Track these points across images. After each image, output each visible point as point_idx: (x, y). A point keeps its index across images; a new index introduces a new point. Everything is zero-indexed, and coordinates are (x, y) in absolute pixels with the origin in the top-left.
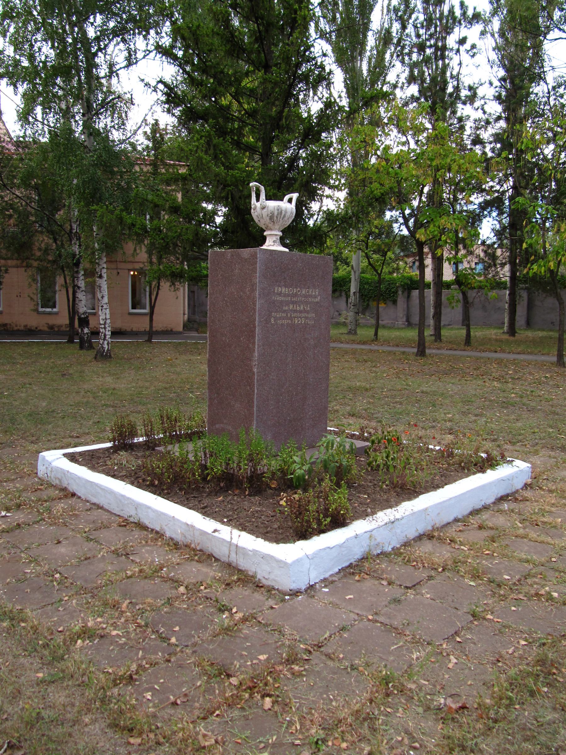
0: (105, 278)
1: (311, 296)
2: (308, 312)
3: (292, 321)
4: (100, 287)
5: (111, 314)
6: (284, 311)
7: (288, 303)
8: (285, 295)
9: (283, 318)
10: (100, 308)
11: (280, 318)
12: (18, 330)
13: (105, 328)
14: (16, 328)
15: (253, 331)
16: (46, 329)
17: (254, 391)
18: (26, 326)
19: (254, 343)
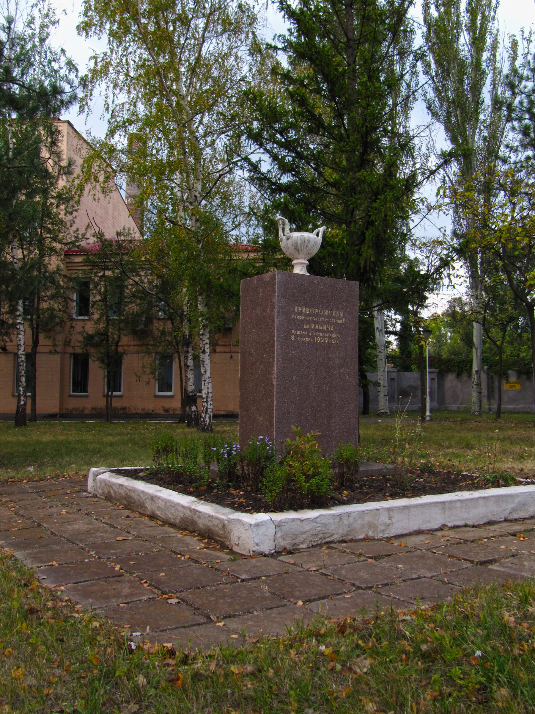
0: (208, 354)
1: (335, 317)
2: (331, 332)
3: (314, 339)
4: (203, 362)
5: (213, 387)
7: (309, 323)
8: (306, 315)
9: (305, 336)
10: (203, 382)
11: (301, 336)
12: (136, 414)
13: (207, 402)
14: (134, 412)
15: (273, 347)
16: (162, 412)
17: (273, 403)
19: (273, 357)
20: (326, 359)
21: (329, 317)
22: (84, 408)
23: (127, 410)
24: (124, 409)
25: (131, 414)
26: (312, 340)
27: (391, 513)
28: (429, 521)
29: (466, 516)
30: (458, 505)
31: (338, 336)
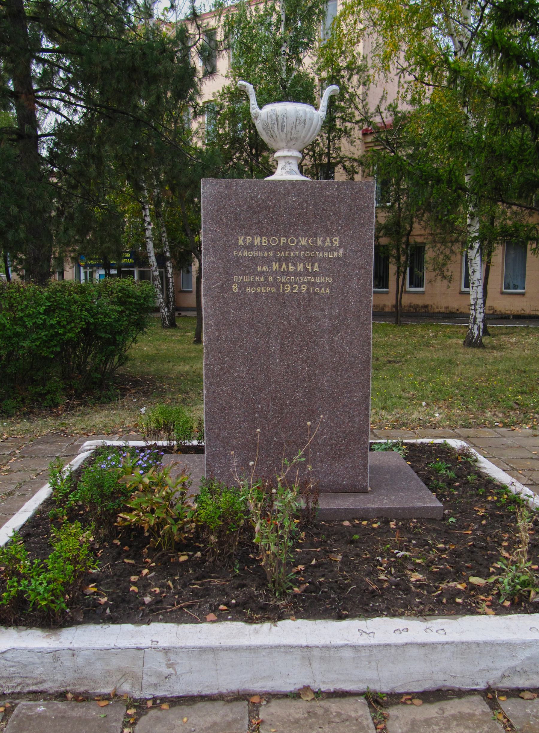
1: (323, 249)
2: (315, 274)
3: (278, 289)
6: (261, 274)
7: (268, 261)
8: (260, 248)
11: (251, 285)
12: (439, 312)
13: (475, 310)
14: (437, 310)
18: (447, 308)
20: (303, 321)
21: (306, 249)
22: (385, 305)
23: (430, 308)
24: (426, 307)
25: (434, 313)
26: (273, 290)
27: (172, 656)
28: (270, 677)
29: (370, 674)
30: (348, 654)
31: (329, 279)
